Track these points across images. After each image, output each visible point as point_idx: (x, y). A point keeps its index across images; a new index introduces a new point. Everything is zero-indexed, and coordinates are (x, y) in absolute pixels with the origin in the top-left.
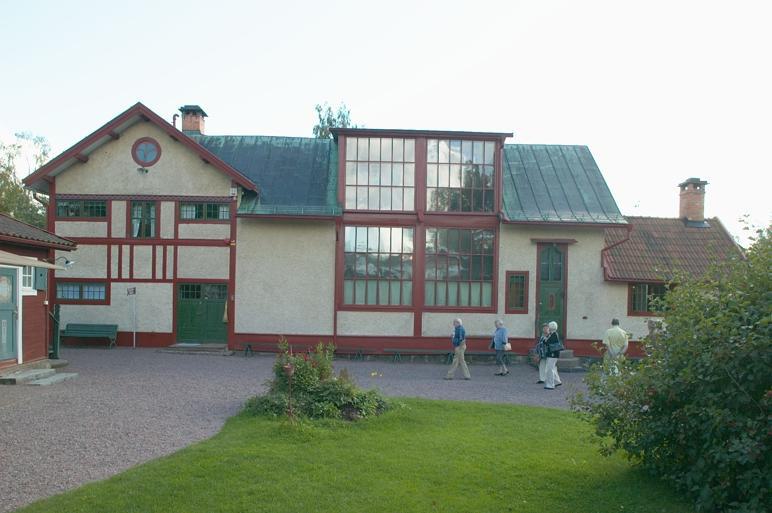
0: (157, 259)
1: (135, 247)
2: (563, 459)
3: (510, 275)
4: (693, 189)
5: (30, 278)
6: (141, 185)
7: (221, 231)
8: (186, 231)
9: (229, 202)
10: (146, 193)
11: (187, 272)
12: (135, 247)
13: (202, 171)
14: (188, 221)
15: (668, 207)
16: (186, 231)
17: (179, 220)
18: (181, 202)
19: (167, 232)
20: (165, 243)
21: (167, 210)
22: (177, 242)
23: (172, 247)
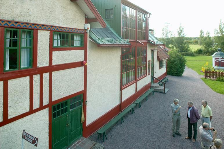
0: (34, 89)
1: (10, 82)
2: (6, 140)
3: (148, 61)
4: (181, 30)
5: (78, 143)
6: (18, 11)
7: (77, 55)
8: (59, 57)
9: (83, 34)
10: (22, 20)
11: (58, 94)
12: (10, 82)
13: (69, 7)
14: (58, 49)
15: (177, 36)
16: (59, 57)
17: (52, 49)
18: (54, 31)
19: (42, 62)
20: (41, 71)
21: (43, 37)
22: (51, 69)
23: (48, 74)
